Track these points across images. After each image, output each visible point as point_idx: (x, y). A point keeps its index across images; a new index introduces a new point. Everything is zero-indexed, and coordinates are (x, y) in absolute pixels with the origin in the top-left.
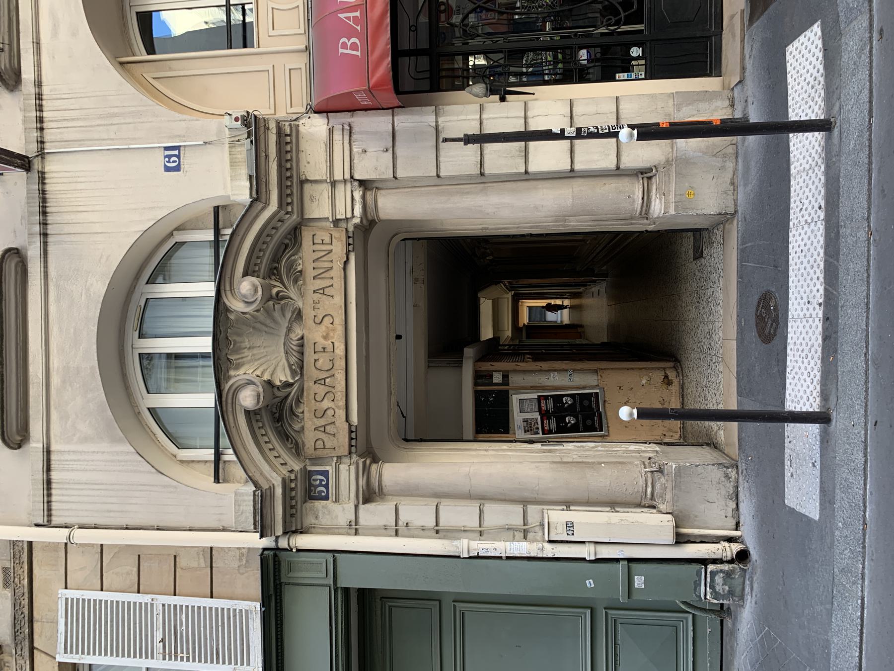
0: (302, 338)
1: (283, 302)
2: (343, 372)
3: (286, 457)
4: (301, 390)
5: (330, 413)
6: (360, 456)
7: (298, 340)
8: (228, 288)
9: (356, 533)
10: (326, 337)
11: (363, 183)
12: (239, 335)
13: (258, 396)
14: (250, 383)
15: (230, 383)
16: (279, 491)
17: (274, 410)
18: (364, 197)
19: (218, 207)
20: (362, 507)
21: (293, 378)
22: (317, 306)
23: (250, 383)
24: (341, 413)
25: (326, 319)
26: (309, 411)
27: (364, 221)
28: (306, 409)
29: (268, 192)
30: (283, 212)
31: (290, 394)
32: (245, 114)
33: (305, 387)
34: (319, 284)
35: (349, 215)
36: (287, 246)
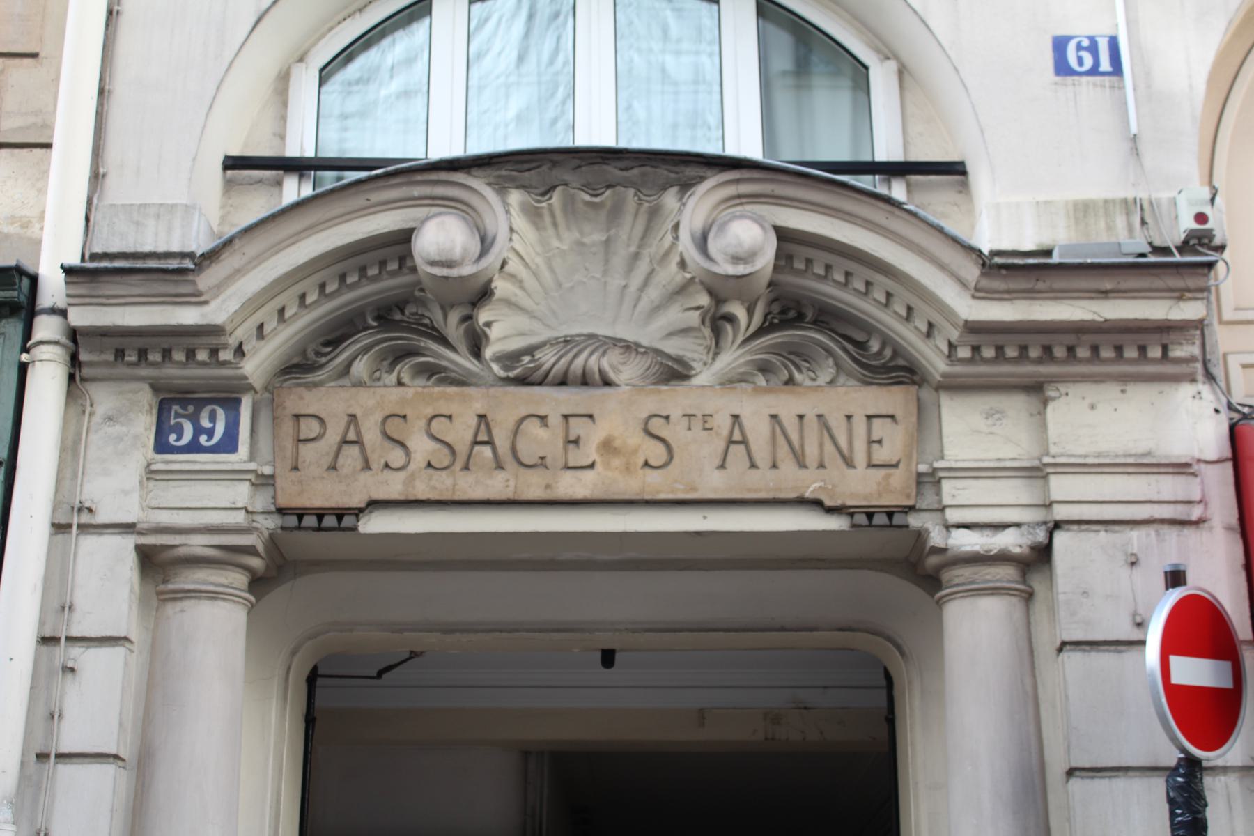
0: (607, 383)
2: (508, 494)
5: (396, 457)
6: (273, 541)
8: (745, 188)
9: (60, 528)
10: (608, 447)
11: (1042, 555)
14: (486, 244)
15: (489, 193)
16: (188, 316)
18: (1002, 558)
20: (127, 544)
22: (697, 424)
23: (486, 244)
24: (393, 487)
25: (660, 448)
32: (1217, 241)
35: (953, 516)
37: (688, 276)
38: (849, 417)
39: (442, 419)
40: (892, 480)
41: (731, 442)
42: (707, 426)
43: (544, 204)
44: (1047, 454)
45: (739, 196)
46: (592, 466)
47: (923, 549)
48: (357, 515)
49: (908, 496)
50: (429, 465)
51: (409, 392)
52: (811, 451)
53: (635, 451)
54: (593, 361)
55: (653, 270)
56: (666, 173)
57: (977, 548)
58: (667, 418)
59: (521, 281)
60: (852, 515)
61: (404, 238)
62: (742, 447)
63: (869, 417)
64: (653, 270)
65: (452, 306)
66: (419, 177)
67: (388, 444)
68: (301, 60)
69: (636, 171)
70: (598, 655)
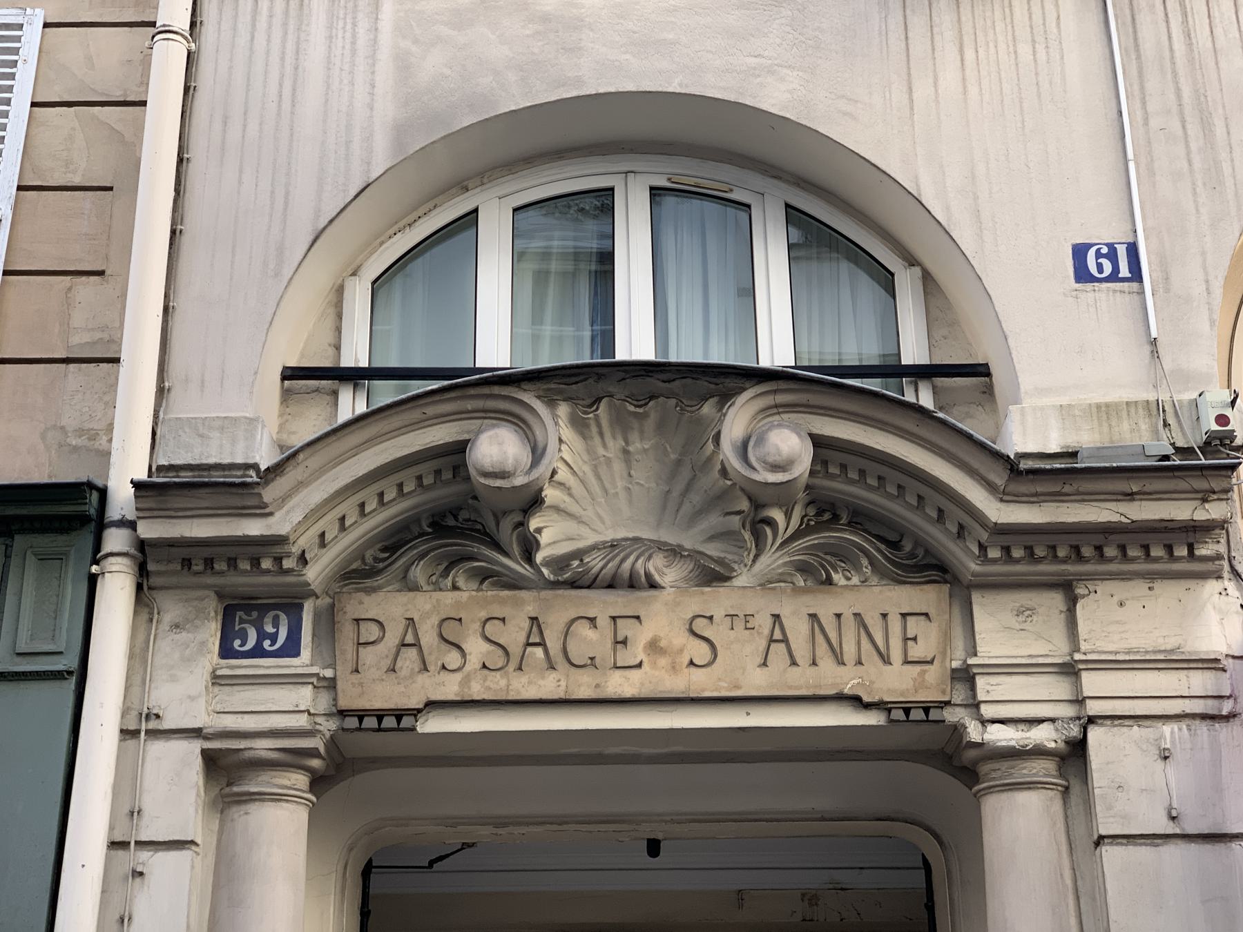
0: (653, 585)
1: (747, 535)
2: (559, 694)
5: (453, 659)
6: (332, 742)
7: (648, 576)
9: (128, 734)
10: (654, 647)
12: (661, 427)
13: (503, 475)
14: (537, 454)
15: (538, 405)
16: (253, 528)
17: (464, 515)
18: (1038, 752)
19: (988, 374)
21: (548, 563)
22: (739, 624)
23: (537, 454)
24: (450, 688)
25: (705, 647)
28: (463, 597)
29: (1035, 499)
30: (984, 536)
33: (523, 594)
34: (798, 630)
35: (987, 711)
39: (496, 622)
40: (927, 677)
41: (772, 640)
42: (749, 625)
44: (1078, 650)
48: (415, 716)
49: (944, 692)
50: (484, 666)
51: (464, 596)
52: (849, 650)
53: (681, 651)
57: (1013, 743)
58: (711, 618)
62: (783, 645)
63: (904, 615)
66: (472, 391)
67: (444, 646)
68: (354, 274)
69: (677, 383)
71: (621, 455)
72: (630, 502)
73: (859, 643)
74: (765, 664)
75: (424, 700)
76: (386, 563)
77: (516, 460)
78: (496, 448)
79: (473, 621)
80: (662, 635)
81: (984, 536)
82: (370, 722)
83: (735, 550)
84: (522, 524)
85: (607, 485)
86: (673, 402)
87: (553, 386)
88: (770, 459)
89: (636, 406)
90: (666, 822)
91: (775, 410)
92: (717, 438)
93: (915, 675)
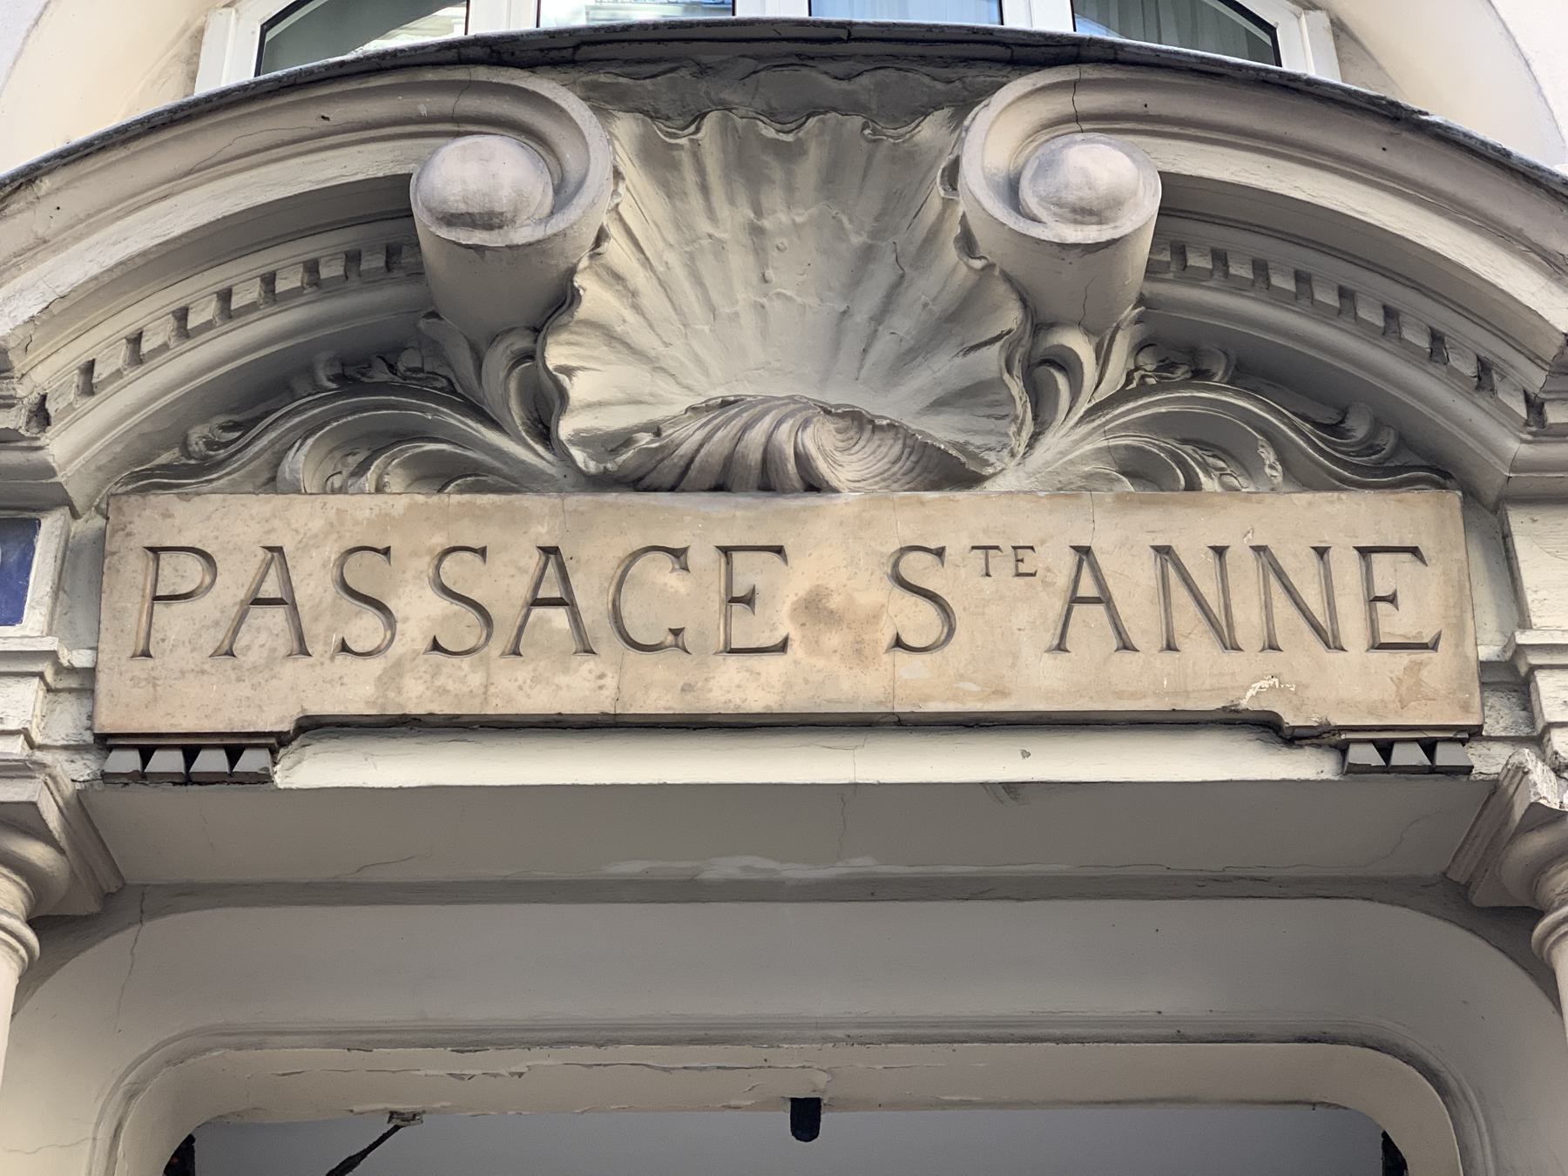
0: (814, 485)
1: (1016, 387)
2: (601, 703)
3: (133, 397)
4: (515, 481)
5: (365, 629)
6: (79, 808)
7: (802, 460)
8: (1089, 101)
10: (814, 608)
12: (830, 180)
13: (489, 220)
14: (563, 191)
15: (571, 103)
17: (408, 360)
22: (1003, 565)
23: (563, 191)
24: (355, 691)
25: (927, 609)
26: (385, 520)
27: (1537, 842)
28: (388, 505)
30: (1537, 379)
31: (495, 425)
33: (528, 501)
36: (1335, 429)
37: (978, 264)
38: (1321, 552)
39: (467, 555)
40: (1424, 674)
41: (1075, 600)
42: (1023, 568)
43: (683, 141)
45: (1077, 118)
46: (782, 647)
47: (1509, 806)
48: (273, 752)
49: (1465, 708)
52: (1247, 620)
53: (874, 617)
54: (784, 434)
55: (902, 276)
56: (927, 80)
59: (634, 294)
60: (1342, 749)
61: (401, 183)
62: (1100, 609)
63: (1365, 552)
64: (902, 276)
65: (494, 339)
66: (430, 75)
69: (865, 80)
70: (785, 1117)
71: (745, 239)
72: (764, 333)
73: (1268, 606)
74: (1061, 647)
75: (296, 713)
76: (232, 449)
77: (520, 194)
78: (471, 172)
79: (415, 554)
80: (832, 586)
81: (1537, 379)
82: (168, 762)
83: (991, 424)
84: (530, 356)
85: (716, 298)
86: (858, 121)
87: (603, 78)
88: (1071, 197)
89: (778, 131)
90: (836, 1041)
91: (1075, 127)
92: (952, 174)
93: (1399, 672)
